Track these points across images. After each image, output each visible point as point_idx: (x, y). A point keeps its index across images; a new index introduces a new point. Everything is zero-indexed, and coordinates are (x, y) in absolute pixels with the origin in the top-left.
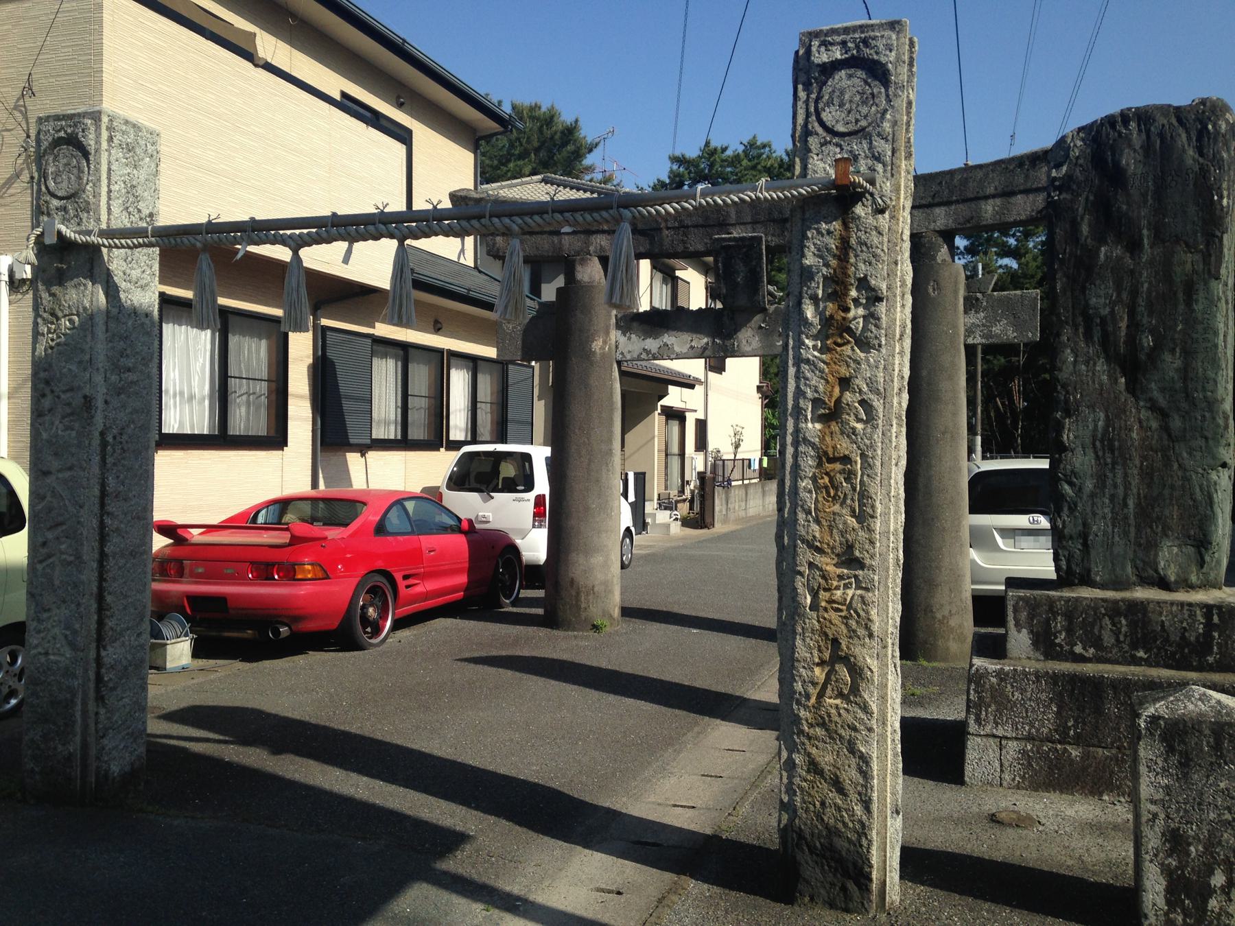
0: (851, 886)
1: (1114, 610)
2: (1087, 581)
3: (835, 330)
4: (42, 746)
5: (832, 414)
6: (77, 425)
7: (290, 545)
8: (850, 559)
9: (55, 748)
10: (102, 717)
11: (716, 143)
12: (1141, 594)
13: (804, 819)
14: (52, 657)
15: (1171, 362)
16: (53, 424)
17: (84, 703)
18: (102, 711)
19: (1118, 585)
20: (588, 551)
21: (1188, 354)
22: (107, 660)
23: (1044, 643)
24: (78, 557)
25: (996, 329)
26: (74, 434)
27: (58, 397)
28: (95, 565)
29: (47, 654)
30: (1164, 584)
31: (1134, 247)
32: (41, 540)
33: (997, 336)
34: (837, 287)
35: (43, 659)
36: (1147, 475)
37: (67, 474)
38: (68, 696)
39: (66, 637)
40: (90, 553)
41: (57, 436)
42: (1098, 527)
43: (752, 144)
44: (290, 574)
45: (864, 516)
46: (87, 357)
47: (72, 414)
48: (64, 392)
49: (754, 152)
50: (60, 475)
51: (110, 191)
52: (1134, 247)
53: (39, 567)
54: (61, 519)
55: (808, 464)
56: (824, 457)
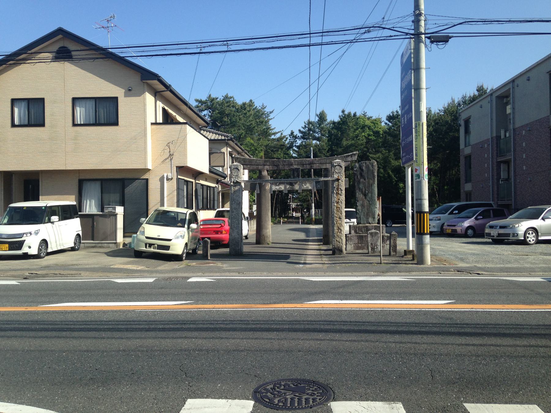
1: (364, 227)
2: (360, 223)
3: (337, 194)
5: (338, 203)
7: (73, 249)
8: (340, 218)
11: (213, 96)
12: (367, 225)
13: (336, 246)
15: (370, 195)
19: (364, 224)
20: (266, 229)
21: (372, 194)
23: (356, 232)
30: (370, 223)
31: (365, 179)
34: (338, 189)
36: (367, 209)
42: (362, 216)
43: (226, 97)
44: (221, 233)
45: (341, 214)
49: (227, 100)
52: (365, 179)
55: (335, 208)
56: (337, 207)
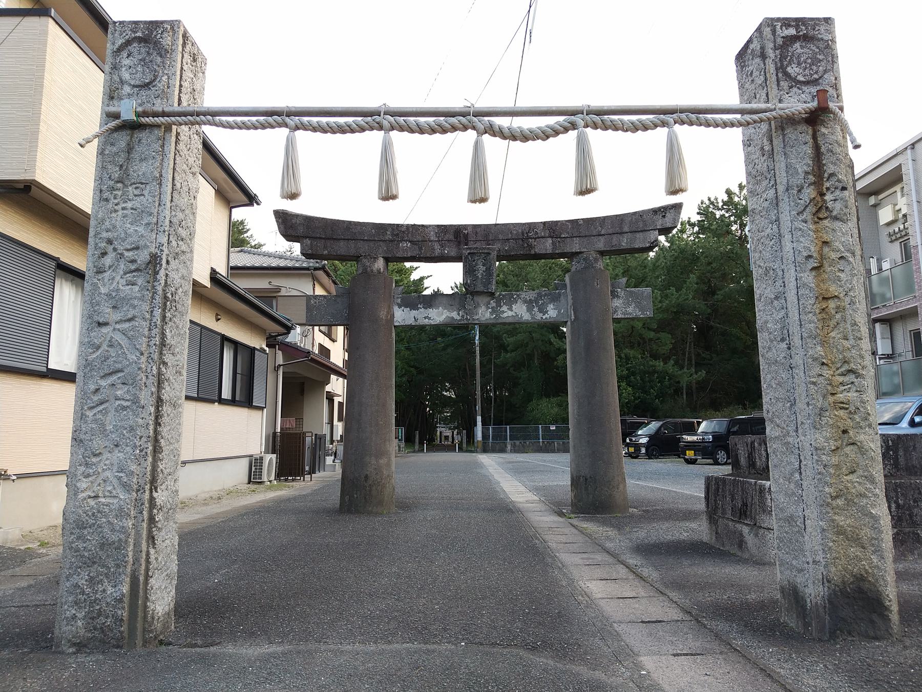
0: (875, 617)
4: (88, 590)
6: (140, 281)
9: (104, 591)
10: (152, 557)
14: (103, 500)
16: (113, 279)
17: (137, 544)
18: (152, 551)
22: (159, 502)
24: (135, 401)
25: (630, 310)
26: (136, 288)
27: (122, 254)
28: (152, 409)
29: (96, 497)
32: (93, 387)
33: (630, 314)
35: (92, 502)
37: (126, 325)
38: (122, 536)
39: (119, 478)
40: (146, 397)
41: (118, 290)
46: (155, 220)
47: (137, 270)
48: (128, 250)
50: (118, 326)
51: (181, 86)
53: (90, 414)
54: (119, 366)
